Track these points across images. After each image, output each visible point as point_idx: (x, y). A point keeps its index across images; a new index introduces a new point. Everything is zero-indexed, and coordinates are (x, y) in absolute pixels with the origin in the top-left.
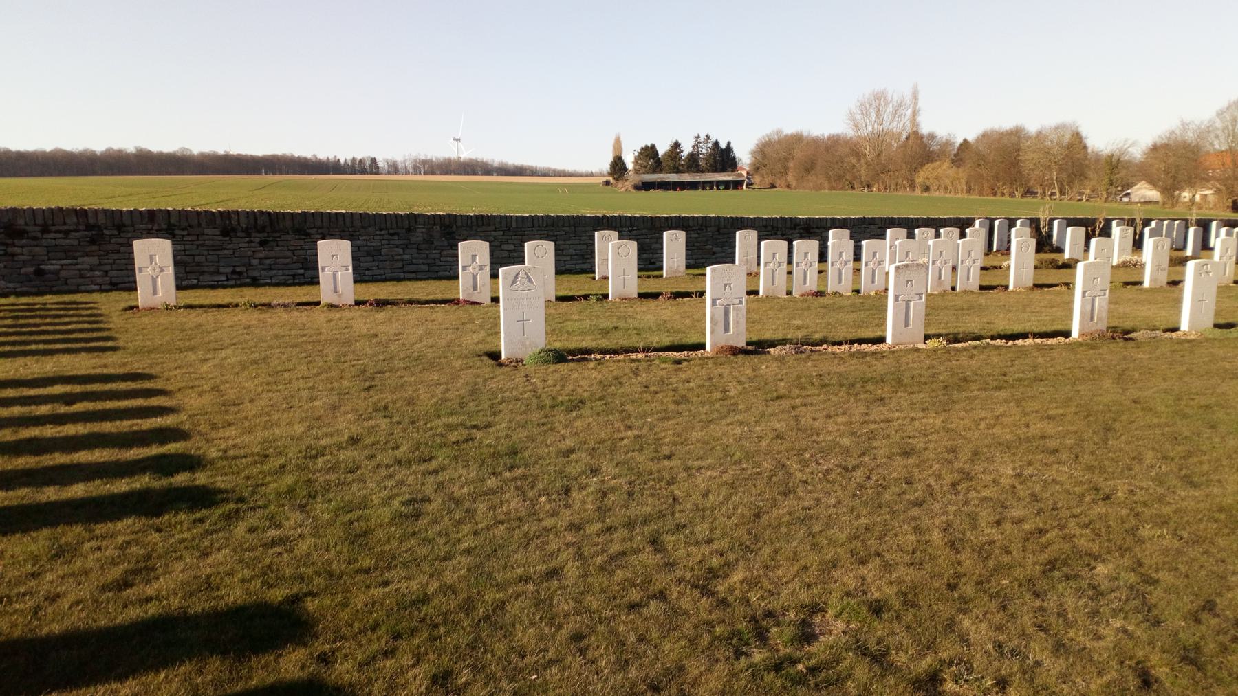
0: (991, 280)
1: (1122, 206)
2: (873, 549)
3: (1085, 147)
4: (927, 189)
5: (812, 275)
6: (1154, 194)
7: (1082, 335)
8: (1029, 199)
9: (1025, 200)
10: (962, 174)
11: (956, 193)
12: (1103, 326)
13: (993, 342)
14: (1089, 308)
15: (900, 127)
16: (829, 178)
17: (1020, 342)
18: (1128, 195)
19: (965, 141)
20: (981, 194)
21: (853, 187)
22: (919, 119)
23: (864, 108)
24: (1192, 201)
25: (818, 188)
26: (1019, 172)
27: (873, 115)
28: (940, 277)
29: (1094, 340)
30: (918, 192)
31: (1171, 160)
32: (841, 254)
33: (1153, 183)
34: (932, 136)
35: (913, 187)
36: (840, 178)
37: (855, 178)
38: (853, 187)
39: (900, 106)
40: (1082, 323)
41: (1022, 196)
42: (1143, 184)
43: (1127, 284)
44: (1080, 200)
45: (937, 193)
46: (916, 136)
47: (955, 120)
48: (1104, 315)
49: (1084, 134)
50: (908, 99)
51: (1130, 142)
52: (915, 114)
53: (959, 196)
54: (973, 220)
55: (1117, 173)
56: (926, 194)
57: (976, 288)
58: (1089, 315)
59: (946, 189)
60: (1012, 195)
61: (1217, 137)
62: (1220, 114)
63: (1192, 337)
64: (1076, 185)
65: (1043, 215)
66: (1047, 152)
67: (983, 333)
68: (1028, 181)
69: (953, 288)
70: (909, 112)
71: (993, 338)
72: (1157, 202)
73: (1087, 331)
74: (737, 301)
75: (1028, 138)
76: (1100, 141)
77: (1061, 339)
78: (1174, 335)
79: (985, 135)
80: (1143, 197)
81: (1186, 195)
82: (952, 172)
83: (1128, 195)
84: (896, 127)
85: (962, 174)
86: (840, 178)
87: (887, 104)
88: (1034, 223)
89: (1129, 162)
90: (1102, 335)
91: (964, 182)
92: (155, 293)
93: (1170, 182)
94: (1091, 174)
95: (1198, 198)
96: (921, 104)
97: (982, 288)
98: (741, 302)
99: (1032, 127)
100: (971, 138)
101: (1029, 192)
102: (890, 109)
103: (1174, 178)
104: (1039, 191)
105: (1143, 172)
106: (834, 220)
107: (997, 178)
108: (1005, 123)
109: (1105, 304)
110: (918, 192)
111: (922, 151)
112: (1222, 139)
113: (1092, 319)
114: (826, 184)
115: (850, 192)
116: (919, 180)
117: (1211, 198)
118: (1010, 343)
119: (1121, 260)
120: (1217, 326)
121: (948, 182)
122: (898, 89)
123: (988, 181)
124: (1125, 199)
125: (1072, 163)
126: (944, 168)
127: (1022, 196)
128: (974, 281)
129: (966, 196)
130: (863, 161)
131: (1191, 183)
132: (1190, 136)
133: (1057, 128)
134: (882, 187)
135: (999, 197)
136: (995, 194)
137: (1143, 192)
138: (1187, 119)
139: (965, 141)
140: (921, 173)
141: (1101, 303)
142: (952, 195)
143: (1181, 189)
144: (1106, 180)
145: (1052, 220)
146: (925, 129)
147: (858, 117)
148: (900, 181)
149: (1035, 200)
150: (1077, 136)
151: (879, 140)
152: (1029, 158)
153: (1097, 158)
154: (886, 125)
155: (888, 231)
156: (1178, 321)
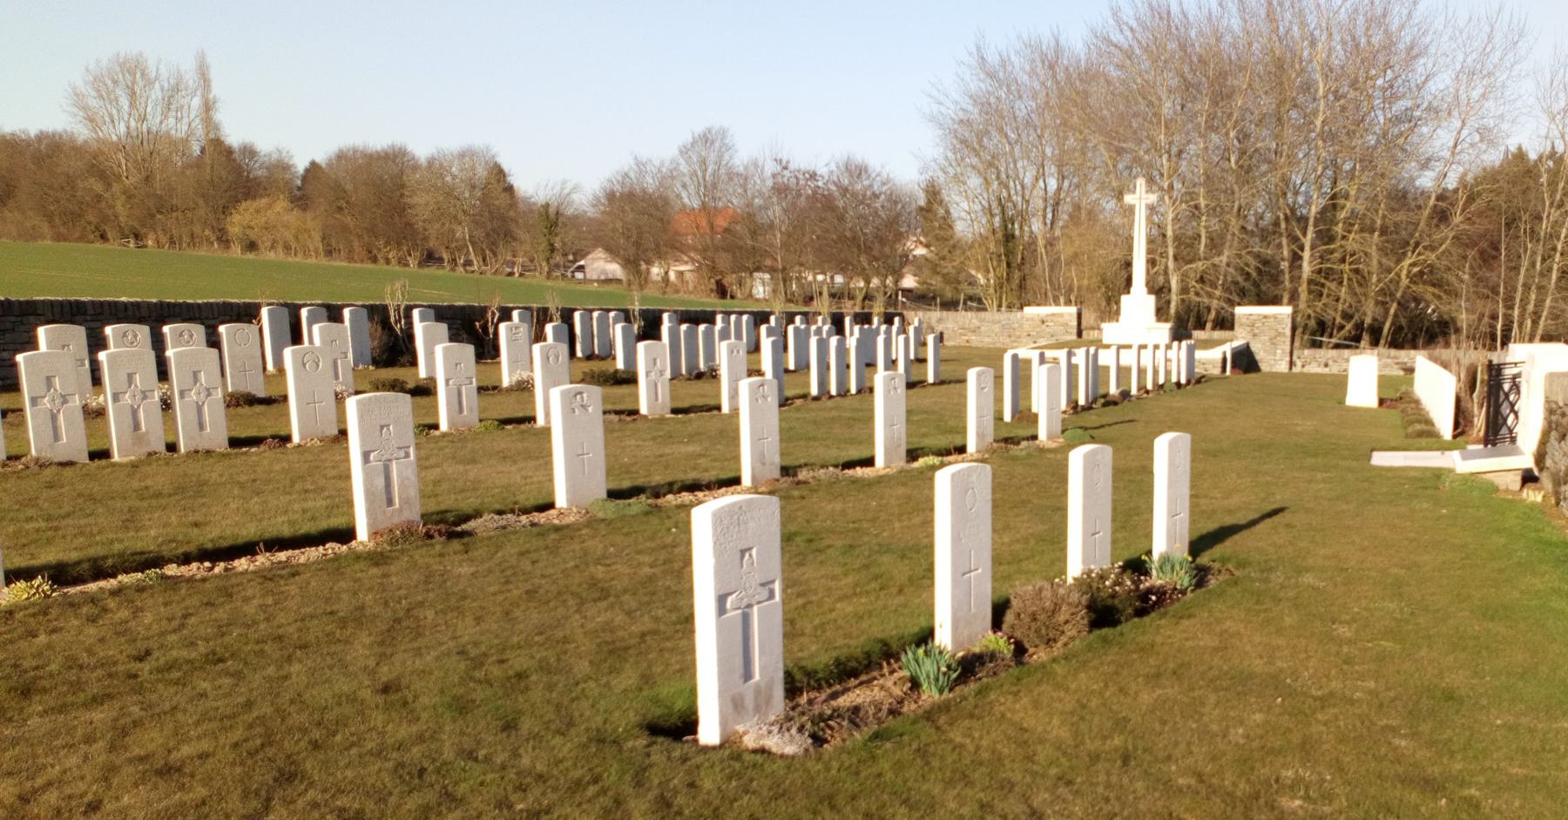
0: (255, 422)
1: (572, 286)
2: (1494, 712)
3: (509, 189)
4: (252, 246)
5: (149, 416)
6: (615, 269)
7: (374, 534)
8: (432, 271)
9: (426, 271)
10: (313, 222)
11: (306, 254)
12: (413, 514)
13: (184, 570)
14: (380, 482)
15: (183, 125)
16: (50, 217)
17: (242, 564)
18: (581, 268)
19: (313, 164)
20: (351, 259)
21: (103, 237)
22: (220, 116)
23: (102, 84)
24: (666, 279)
25: (32, 235)
26: (409, 225)
27: (124, 102)
28: (137, 426)
29: (397, 539)
30: (236, 251)
31: (630, 217)
32: (195, 375)
33: (613, 252)
34: (249, 152)
35: (224, 241)
36: (73, 217)
37: (105, 219)
38: (103, 237)
39: (176, 89)
40: (370, 512)
41: (420, 265)
42: (599, 253)
43: (505, 422)
44: (511, 274)
45: (272, 255)
46: (218, 147)
47: (292, 121)
48: (413, 493)
49: (506, 167)
50: (191, 78)
51: (569, 186)
52: (208, 107)
53: (313, 261)
54: (258, 307)
55: (558, 235)
56: (251, 256)
57: (219, 442)
58: (383, 496)
59: (287, 248)
60: (402, 262)
61: (684, 186)
62: (684, 152)
63: (572, 519)
64: (501, 250)
65: (393, 300)
66: (449, 193)
67: (166, 551)
68: (425, 239)
69: (172, 447)
70: (196, 102)
71: (186, 560)
72: (619, 281)
73: (384, 525)
74: (402, 454)
75: (416, 167)
76: (532, 181)
77: (332, 547)
78: (540, 518)
79: (341, 156)
80: (604, 272)
81: (656, 271)
82: (294, 217)
83: (581, 268)
84: (177, 127)
85: (313, 222)
86: (73, 217)
87: (149, 83)
88: (378, 314)
89: (576, 217)
90: (408, 532)
91: (317, 236)
92: (57, 437)
93: (632, 251)
94: (521, 234)
95: (672, 276)
96: (216, 90)
97: (235, 442)
98: (407, 455)
99: (422, 149)
100: (321, 158)
101: (430, 258)
102: (156, 93)
103: (637, 244)
104: (446, 256)
105: (596, 234)
106: (114, 306)
107: (372, 231)
108: (377, 139)
109: (411, 473)
110: (236, 251)
111: (232, 179)
112: (692, 189)
113: (390, 502)
114: (45, 228)
115: (99, 245)
116: (234, 230)
117: (688, 276)
118: (220, 567)
119: (514, 379)
120: (614, 495)
121: (289, 236)
122: (169, 55)
123: (360, 237)
124: (579, 275)
125: (493, 213)
126: (279, 209)
127: (420, 265)
128: (216, 431)
129: (324, 261)
130: (116, 187)
131: (660, 254)
132: (650, 184)
133: (462, 155)
134: (164, 239)
135: (382, 266)
136: (374, 260)
137: (601, 265)
138: (645, 154)
139: (313, 164)
140: (236, 218)
141: (404, 472)
142: (299, 259)
143: (649, 263)
144: (544, 246)
145: (409, 309)
146: (234, 136)
147: (93, 103)
148: (197, 229)
149: (441, 272)
150: (499, 173)
151: (148, 153)
152: (421, 203)
153: (531, 207)
154: (154, 122)
155: (42, 332)
156: (551, 493)
